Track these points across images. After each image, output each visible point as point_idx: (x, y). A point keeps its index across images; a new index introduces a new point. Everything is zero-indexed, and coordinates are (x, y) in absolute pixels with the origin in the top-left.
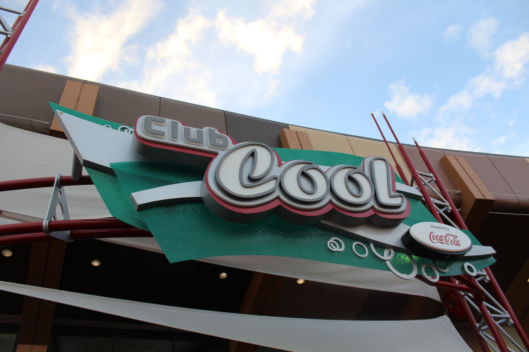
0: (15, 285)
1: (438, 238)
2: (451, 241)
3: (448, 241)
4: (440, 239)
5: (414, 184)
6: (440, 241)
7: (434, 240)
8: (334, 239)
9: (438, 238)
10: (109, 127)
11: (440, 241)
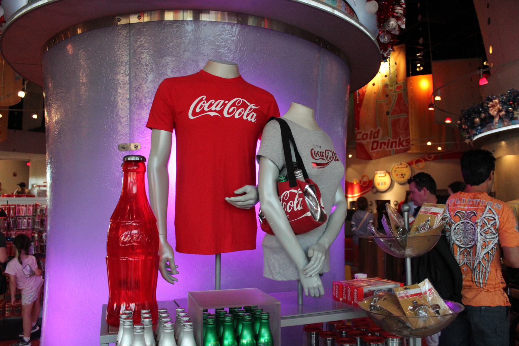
0: (50, 298)
1: (319, 154)
2: (331, 157)
3: (328, 158)
4: (321, 155)
5: (129, 85)
6: (321, 157)
7: (316, 156)
8: (270, 237)
9: (319, 154)
10: (220, 108)
11: (321, 157)
